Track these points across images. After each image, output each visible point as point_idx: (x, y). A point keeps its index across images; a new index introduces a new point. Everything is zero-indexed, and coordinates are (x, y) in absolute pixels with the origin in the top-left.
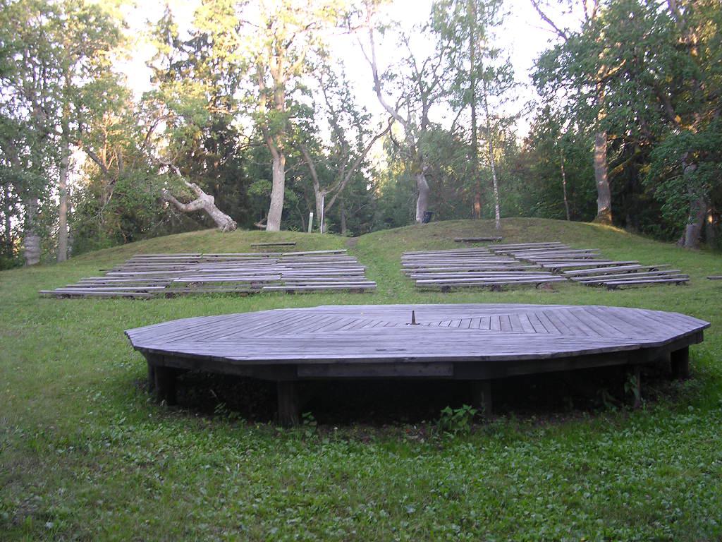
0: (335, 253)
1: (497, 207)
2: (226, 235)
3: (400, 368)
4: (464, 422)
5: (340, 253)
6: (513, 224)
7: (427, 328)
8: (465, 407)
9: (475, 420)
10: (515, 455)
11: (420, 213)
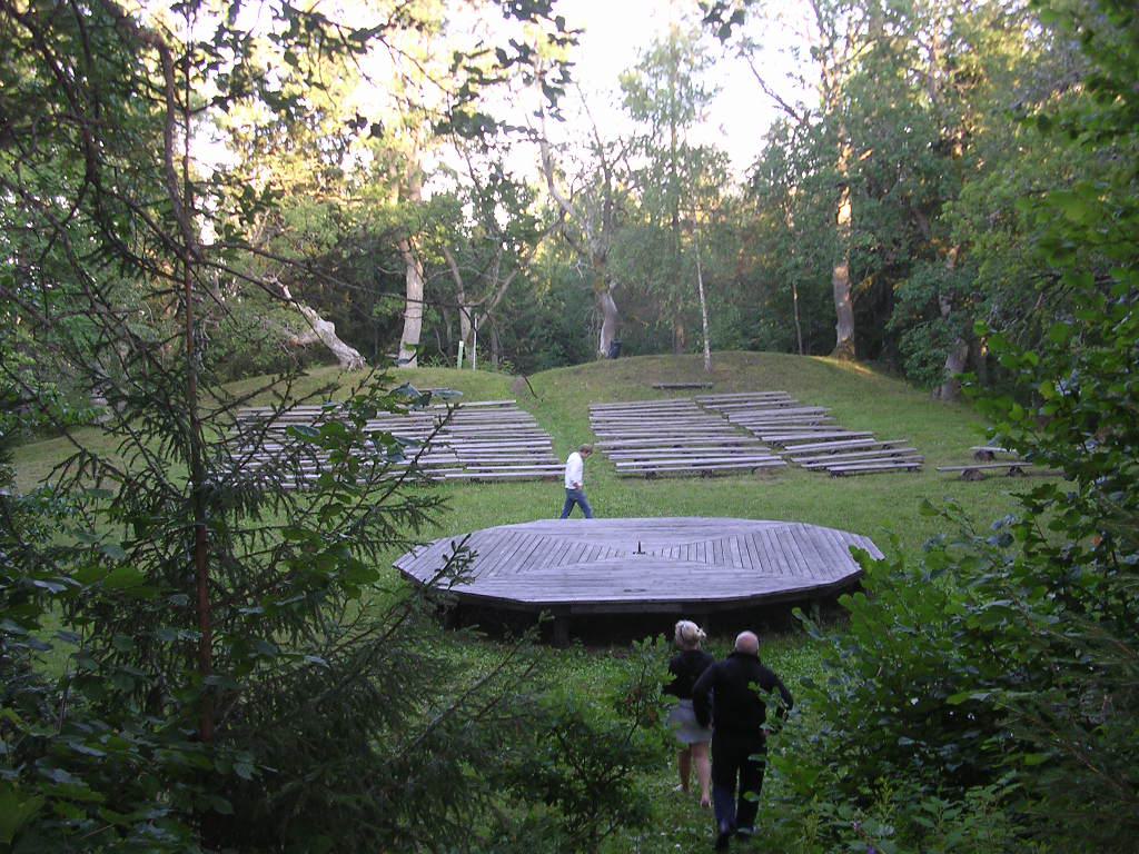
0: (502, 405)
1: (706, 342)
2: (354, 375)
3: (645, 606)
5: (508, 405)
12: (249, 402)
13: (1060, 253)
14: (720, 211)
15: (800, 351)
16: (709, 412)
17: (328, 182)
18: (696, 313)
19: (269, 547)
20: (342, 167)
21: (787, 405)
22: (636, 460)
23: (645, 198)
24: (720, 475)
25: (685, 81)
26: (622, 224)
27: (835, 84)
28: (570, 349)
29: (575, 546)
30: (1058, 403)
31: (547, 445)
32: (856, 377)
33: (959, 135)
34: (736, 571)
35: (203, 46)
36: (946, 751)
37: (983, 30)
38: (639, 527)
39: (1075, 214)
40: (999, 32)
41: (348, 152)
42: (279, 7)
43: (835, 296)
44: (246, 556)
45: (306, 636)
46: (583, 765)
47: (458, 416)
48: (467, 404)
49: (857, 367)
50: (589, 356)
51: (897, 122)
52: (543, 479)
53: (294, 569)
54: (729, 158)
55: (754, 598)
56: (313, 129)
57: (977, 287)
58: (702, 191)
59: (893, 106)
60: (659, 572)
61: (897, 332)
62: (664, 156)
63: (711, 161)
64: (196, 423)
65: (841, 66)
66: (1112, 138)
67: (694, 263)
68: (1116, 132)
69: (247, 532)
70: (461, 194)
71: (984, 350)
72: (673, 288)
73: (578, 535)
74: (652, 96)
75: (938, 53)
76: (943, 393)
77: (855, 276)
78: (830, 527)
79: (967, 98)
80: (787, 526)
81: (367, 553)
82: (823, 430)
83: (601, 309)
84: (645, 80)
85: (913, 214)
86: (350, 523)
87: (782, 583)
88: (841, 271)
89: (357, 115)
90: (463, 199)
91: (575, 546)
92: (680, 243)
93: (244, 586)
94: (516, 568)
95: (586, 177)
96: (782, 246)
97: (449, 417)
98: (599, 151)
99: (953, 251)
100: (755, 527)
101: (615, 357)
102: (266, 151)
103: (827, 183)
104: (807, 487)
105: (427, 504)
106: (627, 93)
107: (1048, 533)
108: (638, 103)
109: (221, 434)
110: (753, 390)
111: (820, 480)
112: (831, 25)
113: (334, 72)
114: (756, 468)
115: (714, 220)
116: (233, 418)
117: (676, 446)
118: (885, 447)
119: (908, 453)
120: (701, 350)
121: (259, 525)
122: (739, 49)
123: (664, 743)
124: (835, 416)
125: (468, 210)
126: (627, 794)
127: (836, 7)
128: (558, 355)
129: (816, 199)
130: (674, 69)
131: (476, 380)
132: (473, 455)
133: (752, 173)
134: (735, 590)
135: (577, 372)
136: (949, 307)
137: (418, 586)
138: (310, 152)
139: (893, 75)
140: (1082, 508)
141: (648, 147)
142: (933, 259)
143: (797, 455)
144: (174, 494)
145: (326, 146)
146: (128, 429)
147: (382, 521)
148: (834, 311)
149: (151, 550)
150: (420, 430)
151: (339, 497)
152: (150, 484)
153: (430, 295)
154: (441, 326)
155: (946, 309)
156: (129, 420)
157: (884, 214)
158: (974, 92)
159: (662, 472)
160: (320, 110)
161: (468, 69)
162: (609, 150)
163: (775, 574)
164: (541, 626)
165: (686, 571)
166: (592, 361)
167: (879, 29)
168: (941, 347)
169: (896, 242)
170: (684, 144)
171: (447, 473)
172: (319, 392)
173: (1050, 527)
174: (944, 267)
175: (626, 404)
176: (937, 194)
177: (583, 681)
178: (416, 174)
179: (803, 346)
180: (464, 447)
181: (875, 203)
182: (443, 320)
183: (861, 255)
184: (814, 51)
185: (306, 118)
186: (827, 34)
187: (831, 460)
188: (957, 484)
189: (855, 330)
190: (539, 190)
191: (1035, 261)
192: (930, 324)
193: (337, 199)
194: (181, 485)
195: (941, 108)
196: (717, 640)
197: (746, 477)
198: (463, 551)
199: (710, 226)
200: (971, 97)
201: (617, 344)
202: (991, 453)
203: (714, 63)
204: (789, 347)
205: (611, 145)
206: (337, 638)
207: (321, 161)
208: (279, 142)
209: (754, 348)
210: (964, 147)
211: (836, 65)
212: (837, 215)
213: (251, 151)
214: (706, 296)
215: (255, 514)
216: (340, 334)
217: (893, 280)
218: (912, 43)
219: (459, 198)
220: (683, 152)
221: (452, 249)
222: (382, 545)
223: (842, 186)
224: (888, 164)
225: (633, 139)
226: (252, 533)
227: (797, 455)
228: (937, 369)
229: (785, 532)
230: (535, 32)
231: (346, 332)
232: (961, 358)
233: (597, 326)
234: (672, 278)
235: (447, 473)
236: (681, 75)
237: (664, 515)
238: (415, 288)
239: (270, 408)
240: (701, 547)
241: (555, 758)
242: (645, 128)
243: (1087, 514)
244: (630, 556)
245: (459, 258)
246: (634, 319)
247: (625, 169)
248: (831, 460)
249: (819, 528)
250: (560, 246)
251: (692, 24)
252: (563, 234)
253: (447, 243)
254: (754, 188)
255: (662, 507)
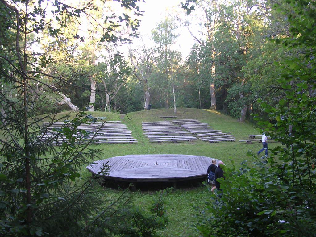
0: (117, 122)
1: (175, 105)
4: (171, 190)
6: (180, 110)
7: (160, 166)
8: (172, 187)
9: (173, 190)
10: (181, 197)
11: (147, 105)
12: (43, 120)
13: (287, 78)
14: (179, 69)
15: (201, 108)
16: (176, 125)
17: (69, 59)
18: (172, 97)
19: (48, 164)
20: (73, 55)
21: (197, 123)
22: (155, 138)
23: (158, 65)
24: (179, 142)
25: (170, 32)
26: (151, 72)
27: (211, 34)
28: (137, 107)
29: (138, 162)
30: (281, 123)
31: (130, 134)
32: (216, 115)
33: (245, 48)
34: (184, 170)
35: (31, 13)
36: (249, 225)
37: (252, 20)
38: (156, 157)
39: (292, 67)
40: (256, 20)
41: (75, 51)
42: (54, 2)
43: (211, 93)
44: (41, 167)
45: (59, 191)
46: (141, 228)
47: (105, 125)
48: (108, 122)
49: (217, 112)
50: (142, 109)
51: (228, 44)
52: (129, 143)
53: (55, 171)
54: (181, 54)
55: (189, 177)
56: (65, 44)
57: (251, 90)
58: (174, 63)
59: (227, 40)
60: (162, 170)
61: (228, 103)
62: (163, 53)
63: (177, 55)
64: (26, 127)
65: (213, 29)
66: (297, 46)
67: (171, 83)
68: (299, 44)
69: (42, 159)
70: (107, 63)
71: (252, 108)
72: (166, 90)
73: (139, 159)
74: (160, 36)
75: (240, 26)
76: (240, 120)
77: (216, 87)
78: (210, 157)
79: (247, 38)
80: (198, 157)
81: (78, 166)
82: (207, 130)
83: (145, 95)
84: (159, 32)
85: (232, 70)
86: (73, 157)
87: (197, 173)
88: (212, 86)
89: (76, 35)
90: (107, 64)
91: (138, 162)
92: (168, 77)
93: (40, 176)
94: (121, 169)
95: (142, 59)
96: (196, 79)
97: (103, 125)
98: (145, 52)
99: (243, 80)
100: (189, 157)
101: (149, 109)
102: (52, 50)
103: (209, 61)
104: (203, 146)
105: (96, 151)
106: (153, 36)
107: (278, 161)
108: (157, 38)
109: (34, 130)
110: (188, 119)
111: (207, 144)
112: (210, 18)
113: (72, 28)
114: (189, 140)
115: (177, 72)
116: (38, 125)
117: (166, 134)
118: (225, 135)
119: (231, 136)
120: (173, 107)
121: (45, 157)
122: (185, 24)
123: (165, 221)
124: (211, 126)
125: (109, 67)
126: (154, 236)
127: (212, 13)
128: (133, 108)
129: (206, 65)
130: (167, 29)
131: (110, 115)
132: (109, 136)
133: (188, 58)
134: (183, 175)
135: (139, 113)
136: (242, 96)
137: (94, 174)
138: (64, 50)
139: (227, 32)
140: (287, 153)
141: (159, 50)
142: (238, 83)
143: (200, 137)
144: (20, 148)
145: (69, 49)
146: (6, 128)
147: (82, 156)
148: (210, 97)
149: (13, 164)
150: (94, 129)
151: (69, 149)
152: (13, 145)
153: (98, 91)
154: (101, 99)
155: (241, 96)
156: (6, 125)
157: (224, 70)
158: (249, 37)
159: (162, 141)
160: (67, 39)
161: (110, 22)
162: (148, 51)
163: (195, 171)
164: (130, 188)
165: (170, 170)
166: (143, 110)
167: (223, 19)
168: (240, 107)
169: (228, 78)
170: (169, 50)
171: (102, 141)
172: (64, 118)
173: (279, 159)
174: (241, 85)
175: (152, 122)
176: (239, 65)
177: (140, 201)
178: (94, 57)
179: (202, 106)
180: (106, 134)
181: (222, 67)
182: (101, 98)
183: (218, 81)
184: (205, 25)
185: (63, 41)
186: (209, 20)
187: (210, 138)
188: (245, 145)
189: (216, 102)
190: (128, 62)
191: (267, 83)
192: (237, 101)
193: (72, 64)
194: (22, 145)
195: (240, 41)
196: (179, 189)
197: (186, 143)
198: (106, 166)
199: (176, 73)
200: (249, 38)
201: (150, 106)
202: (254, 136)
203: (178, 28)
204: (198, 107)
205: (149, 50)
206: (69, 191)
207: (67, 53)
208: (55, 47)
209: (188, 107)
210: (247, 52)
211: (211, 28)
212: (211, 70)
213: (48, 50)
214: (175, 92)
215: (44, 154)
216: (72, 102)
217: (227, 88)
218: (232, 23)
219: (106, 64)
220: (169, 52)
221: (104, 78)
222: (82, 164)
223: (213, 62)
224: (226, 56)
225: (155, 48)
226: (43, 159)
227: (200, 137)
228: (239, 113)
229: (197, 159)
230: (131, 12)
231: (73, 101)
232: (246, 110)
233: (144, 100)
234: (165, 87)
235: (102, 141)
236: (169, 31)
237: (163, 154)
238: (93, 87)
239: (49, 123)
240: (174, 163)
241: (133, 226)
242: (158, 45)
243: (289, 155)
244: (154, 165)
245: (106, 81)
246: (154, 98)
247: (153, 57)
248: (210, 138)
249: (207, 158)
250: (134, 78)
251: (172, 17)
252: (135, 74)
253: (103, 76)
254: (188, 63)
255: (162, 151)
